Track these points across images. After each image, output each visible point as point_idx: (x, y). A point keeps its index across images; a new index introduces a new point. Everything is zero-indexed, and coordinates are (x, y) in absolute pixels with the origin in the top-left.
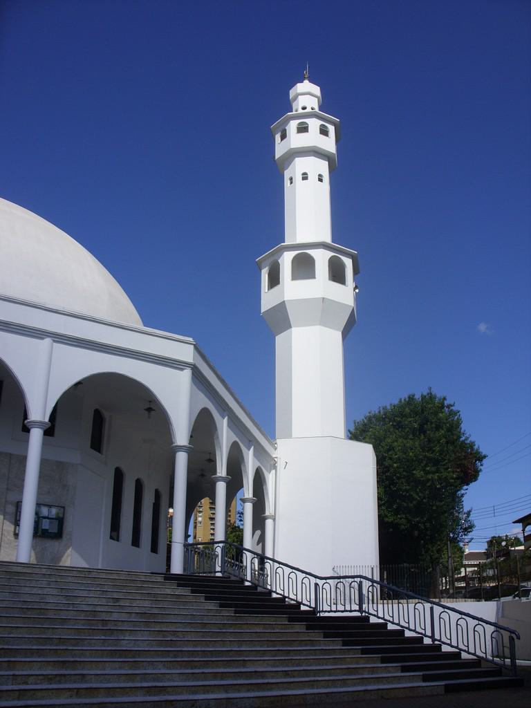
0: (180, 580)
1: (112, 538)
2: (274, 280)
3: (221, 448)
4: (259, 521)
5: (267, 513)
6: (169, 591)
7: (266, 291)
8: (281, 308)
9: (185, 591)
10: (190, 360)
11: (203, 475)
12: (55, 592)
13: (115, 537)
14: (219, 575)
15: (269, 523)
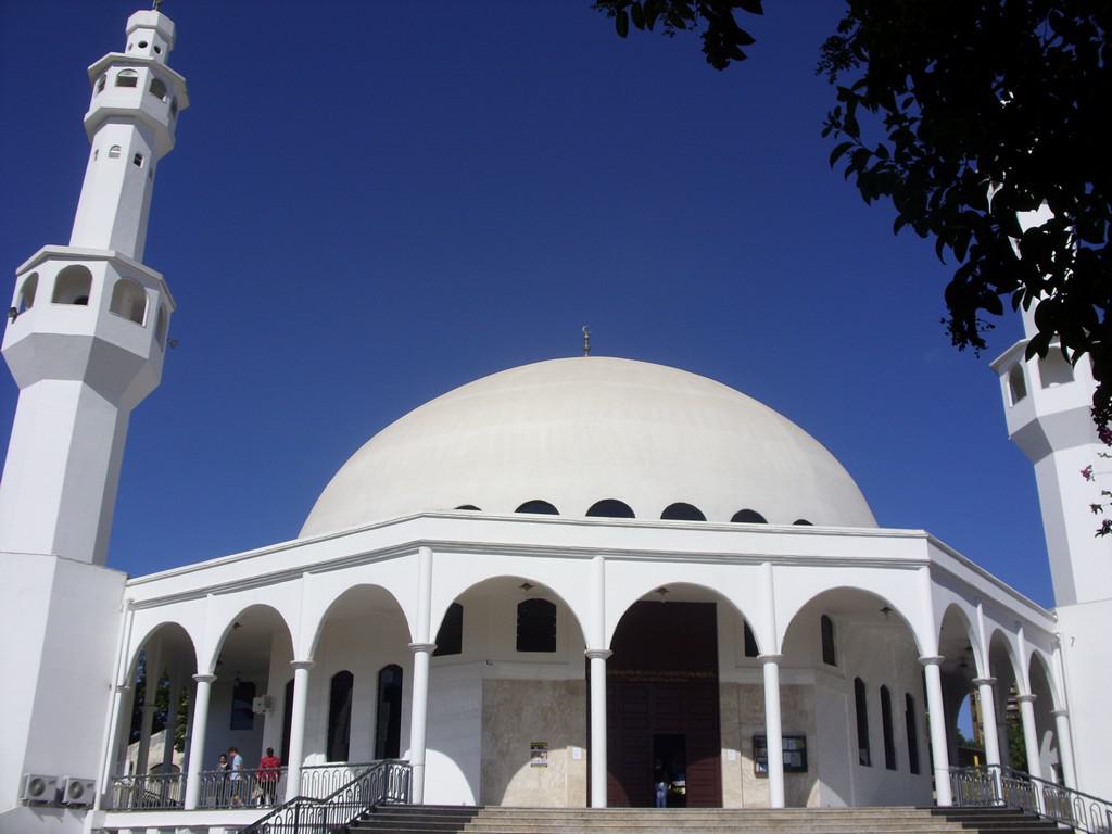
0: (950, 814)
1: (862, 762)
2: (1019, 390)
3: (979, 645)
4: (1046, 719)
5: (1057, 708)
6: (938, 828)
7: (1011, 405)
8: (1034, 427)
9: (956, 827)
10: (925, 556)
11: (964, 665)
12: (716, 818)
13: (866, 761)
14: (1001, 803)
15: (1061, 722)
